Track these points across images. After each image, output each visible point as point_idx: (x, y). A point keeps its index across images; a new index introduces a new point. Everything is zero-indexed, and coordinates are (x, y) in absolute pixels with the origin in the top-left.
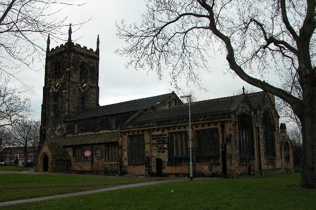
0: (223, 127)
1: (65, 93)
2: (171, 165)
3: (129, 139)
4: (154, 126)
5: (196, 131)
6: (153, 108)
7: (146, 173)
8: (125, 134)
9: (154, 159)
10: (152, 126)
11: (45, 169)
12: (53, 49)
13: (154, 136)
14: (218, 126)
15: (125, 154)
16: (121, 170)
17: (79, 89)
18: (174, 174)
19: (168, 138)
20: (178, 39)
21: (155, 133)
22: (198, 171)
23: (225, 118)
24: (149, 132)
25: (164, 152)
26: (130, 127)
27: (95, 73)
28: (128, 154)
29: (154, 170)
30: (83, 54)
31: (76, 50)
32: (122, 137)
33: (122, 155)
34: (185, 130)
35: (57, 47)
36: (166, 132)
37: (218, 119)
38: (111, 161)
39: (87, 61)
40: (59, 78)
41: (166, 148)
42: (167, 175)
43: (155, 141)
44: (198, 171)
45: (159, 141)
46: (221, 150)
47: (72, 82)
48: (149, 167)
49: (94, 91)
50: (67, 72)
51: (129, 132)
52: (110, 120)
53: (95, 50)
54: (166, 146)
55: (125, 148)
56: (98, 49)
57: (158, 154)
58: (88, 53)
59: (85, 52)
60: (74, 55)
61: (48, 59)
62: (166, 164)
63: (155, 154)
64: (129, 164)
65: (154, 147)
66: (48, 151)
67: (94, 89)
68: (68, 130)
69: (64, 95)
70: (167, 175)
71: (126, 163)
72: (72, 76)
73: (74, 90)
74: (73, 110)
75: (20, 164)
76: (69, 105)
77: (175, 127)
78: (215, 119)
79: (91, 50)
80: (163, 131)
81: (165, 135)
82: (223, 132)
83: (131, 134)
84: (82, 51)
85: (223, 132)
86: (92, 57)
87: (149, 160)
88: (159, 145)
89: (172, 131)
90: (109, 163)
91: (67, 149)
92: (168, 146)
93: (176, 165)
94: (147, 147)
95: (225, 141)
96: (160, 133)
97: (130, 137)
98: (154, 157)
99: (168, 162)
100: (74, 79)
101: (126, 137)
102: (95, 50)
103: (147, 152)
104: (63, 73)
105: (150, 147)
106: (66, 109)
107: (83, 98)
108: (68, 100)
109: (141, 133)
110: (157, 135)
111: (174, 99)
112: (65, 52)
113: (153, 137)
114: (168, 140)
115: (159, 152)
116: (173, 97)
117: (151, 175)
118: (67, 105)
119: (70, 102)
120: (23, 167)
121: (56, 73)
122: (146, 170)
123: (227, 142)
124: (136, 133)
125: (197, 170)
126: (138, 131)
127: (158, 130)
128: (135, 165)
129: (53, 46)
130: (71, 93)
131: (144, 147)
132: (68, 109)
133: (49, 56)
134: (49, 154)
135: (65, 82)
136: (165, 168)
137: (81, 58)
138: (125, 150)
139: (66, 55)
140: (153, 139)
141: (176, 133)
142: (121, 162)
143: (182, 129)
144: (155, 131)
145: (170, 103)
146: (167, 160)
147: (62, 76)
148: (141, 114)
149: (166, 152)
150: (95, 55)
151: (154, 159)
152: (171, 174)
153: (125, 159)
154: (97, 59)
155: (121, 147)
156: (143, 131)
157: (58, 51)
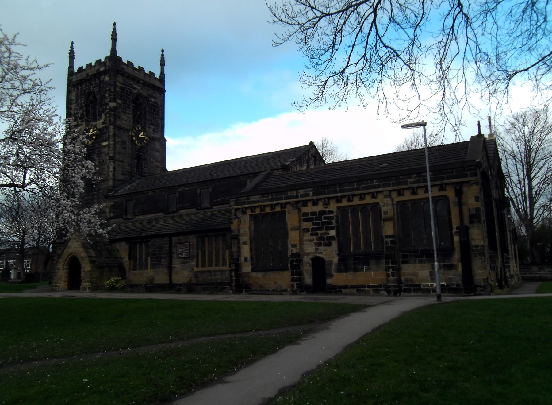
0: (459, 193)
1: (108, 146)
2: (346, 271)
3: (253, 222)
4: (308, 195)
5: (398, 202)
6: (285, 168)
7: (293, 286)
8: (244, 213)
9: (307, 259)
10: (302, 196)
11: (466, 156)
12: (81, 69)
13: (306, 214)
14: (450, 193)
15: (246, 251)
16: (237, 281)
17: (132, 140)
18: (352, 287)
19: (337, 217)
20: (324, 45)
21: (310, 209)
22: (406, 280)
23: (466, 176)
24: (297, 208)
25: (329, 245)
26: (255, 198)
27: (158, 115)
28: (251, 250)
29: (308, 280)
30: (137, 80)
31: (126, 71)
32: (238, 218)
33: (239, 252)
34: (374, 201)
35: (89, 65)
36: (333, 206)
37: (448, 178)
38: (203, 266)
39: (145, 93)
40: (95, 120)
41: (333, 238)
42: (336, 290)
43: (309, 225)
44: (406, 280)
45: (318, 224)
46: (456, 239)
47: (120, 128)
48: (300, 274)
49: (158, 146)
50: (110, 110)
51: (253, 209)
52: (198, 192)
53: (157, 75)
54: (333, 233)
55: (245, 238)
56: (162, 73)
57: (317, 249)
58: (147, 79)
59: (141, 76)
60: (122, 81)
61: (72, 86)
62: (334, 267)
63: (310, 248)
64: (253, 270)
65: (307, 236)
66: (81, 249)
67: (157, 143)
68: (114, 212)
69: (106, 150)
70: (336, 290)
71: (247, 268)
72: (119, 117)
73: (124, 142)
74: (121, 177)
75: (12, 277)
76: (114, 168)
77: (353, 195)
78: (442, 179)
79: (152, 74)
80: (326, 204)
81: (331, 212)
82: (460, 204)
83: (258, 211)
84: (136, 74)
85: (460, 204)
86: (154, 87)
87: (300, 261)
88: (320, 232)
89: (345, 203)
90: (218, 268)
91: (117, 246)
92: (338, 233)
93: (356, 270)
94: (293, 236)
95: (466, 221)
96: (319, 208)
97: (254, 218)
98: (308, 254)
99: (339, 264)
100: (123, 122)
101: (246, 219)
102: (157, 75)
103: (294, 246)
104: (103, 112)
105: (300, 234)
106: (109, 175)
107: (139, 158)
108: (111, 158)
109: (278, 209)
110: (313, 214)
111: (313, 156)
112: (105, 73)
113: (306, 218)
114: (337, 222)
115: (319, 244)
116: (312, 152)
117: (302, 288)
118: (111, 168)
119: (117, 162)
120: (21, 282)
121: (87, 112)
122: (293, 280)
123: (471, 222)
124: (268, 210)
125: (403, 279)
126: (273, 207)
127: (315, 203)
128: (265, 270)
129: (80, 63)
130: (118, 146)
131: (286, 236)
132: (114, 175)
133: (74, 80)
134: (83, 254)
135: (107, 127)
136: (331, 276)
137: (135, 86)
138: (245, 243)
139: (107, 79)
140: (306, 220)
141: (354, 208)
142: (236, 262)
143: (368, 200)
144: (310, 204)
145: (308, 162)
146: (336, 260)
147: (100, 115)
148: (268, 176)
149: (335, 244)
150: (158, 84)
151: (307, 259)
152: (346, 287)
153: (246, 259)
154: (162, 91)
155: (237, 238)
156: (283, 206)
157: (91, 72)
